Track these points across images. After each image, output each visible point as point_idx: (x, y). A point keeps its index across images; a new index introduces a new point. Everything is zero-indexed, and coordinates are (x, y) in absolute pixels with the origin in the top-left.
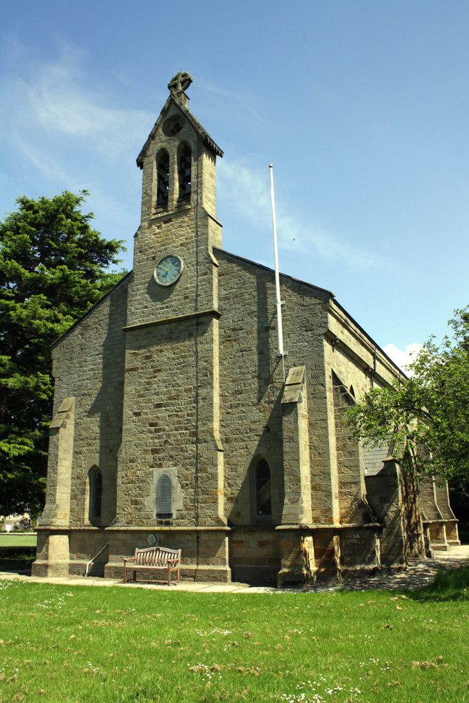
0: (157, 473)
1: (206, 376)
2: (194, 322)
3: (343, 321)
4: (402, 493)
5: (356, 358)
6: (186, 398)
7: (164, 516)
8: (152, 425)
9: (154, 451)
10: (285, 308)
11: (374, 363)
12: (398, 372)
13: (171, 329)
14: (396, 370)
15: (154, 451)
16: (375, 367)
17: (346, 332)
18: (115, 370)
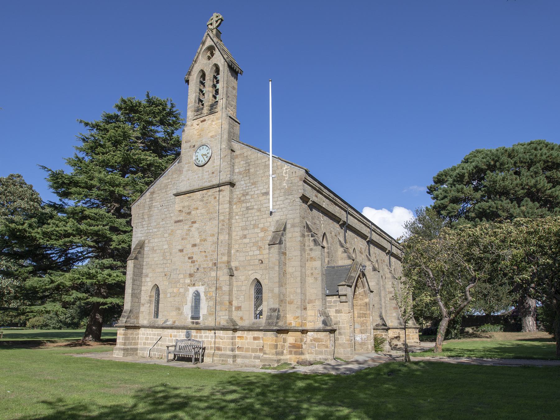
0: (192, 290)
1: (224, 225)
2: (218, 189)
3: (317, 188)
4: (57, 353)
5: (330, 214)
6: (227, 221)
7: (195, 317)
8: (189, 258)
9: (191, 275)
10: (276, 179)
11: (347, 217)
12: (370, 224)
13: (203, 195)
14: (368, 222)
15: (191, 275)
16: (347, 220)
17: (320, 195)
18: (169, 222)
